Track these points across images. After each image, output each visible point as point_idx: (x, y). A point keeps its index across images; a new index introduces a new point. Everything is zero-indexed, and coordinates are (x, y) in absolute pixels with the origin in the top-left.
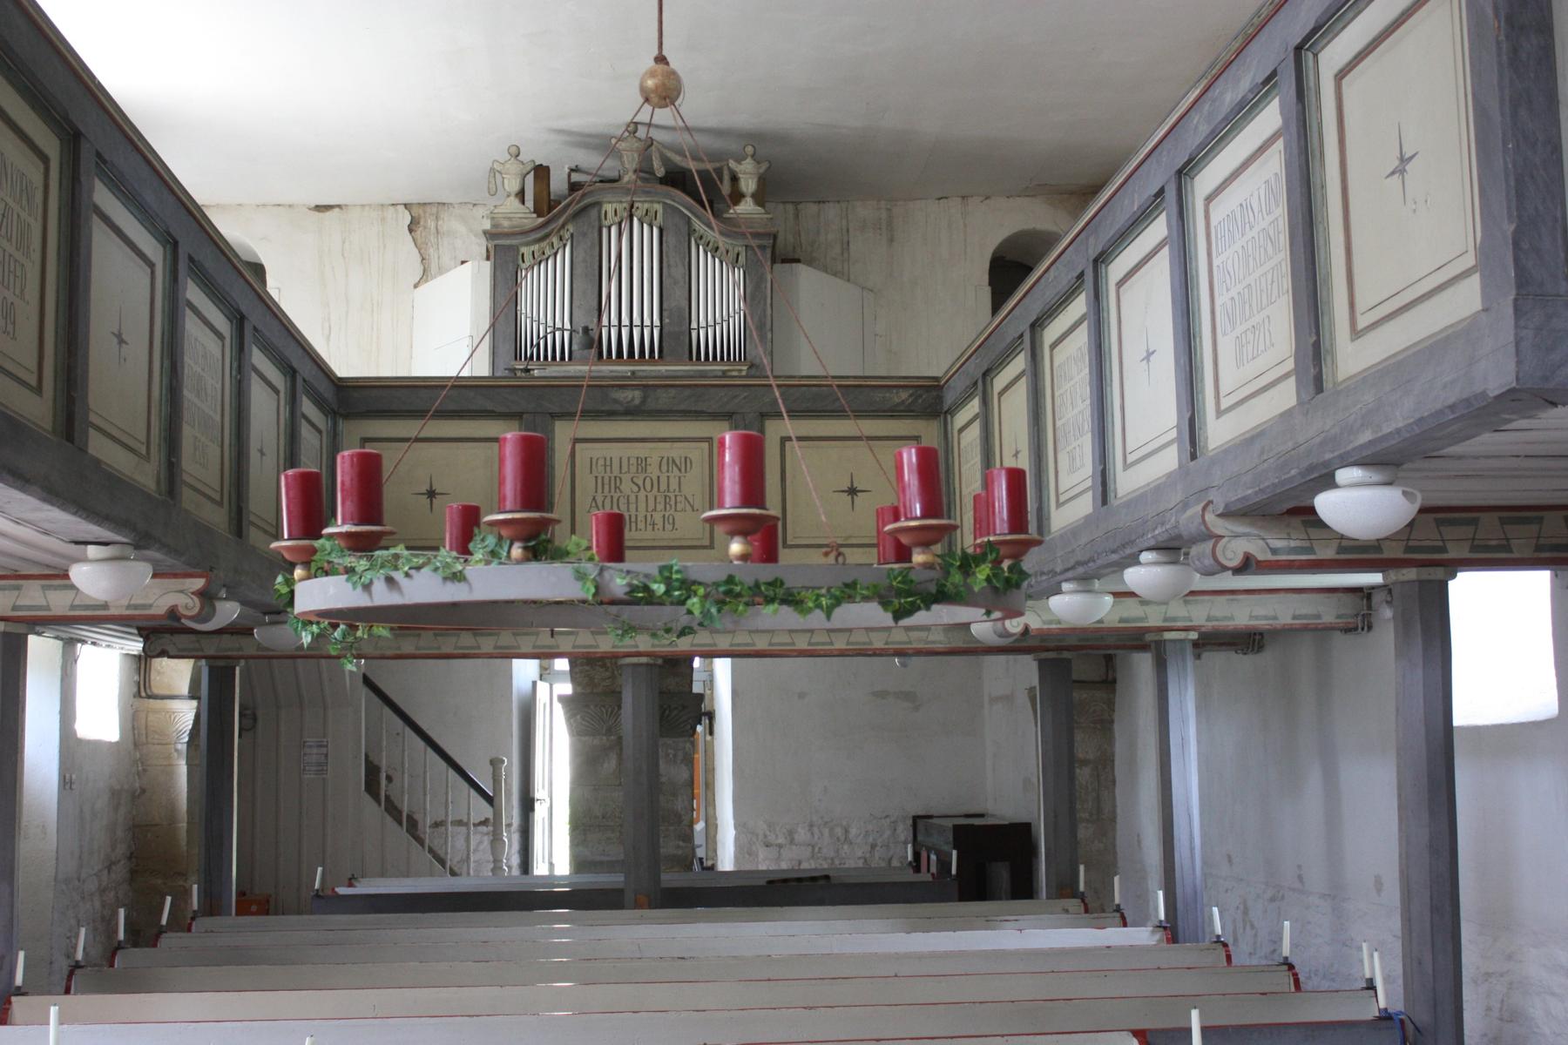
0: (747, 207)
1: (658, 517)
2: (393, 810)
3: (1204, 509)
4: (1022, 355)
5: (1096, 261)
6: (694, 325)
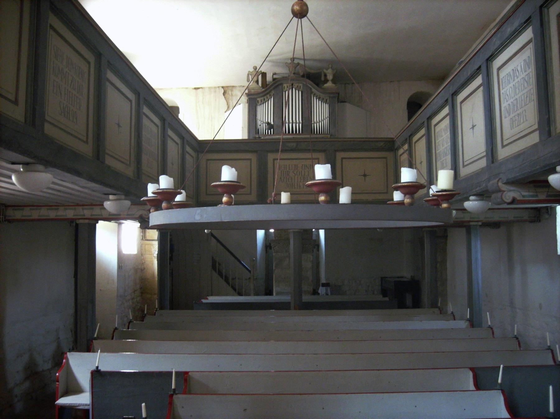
0: (329, 84)
1: (301, 184)
2: (220, 274)
3: (498, 181)
4: (424, 129)
5: (452, 95)
6: (313, 122)
